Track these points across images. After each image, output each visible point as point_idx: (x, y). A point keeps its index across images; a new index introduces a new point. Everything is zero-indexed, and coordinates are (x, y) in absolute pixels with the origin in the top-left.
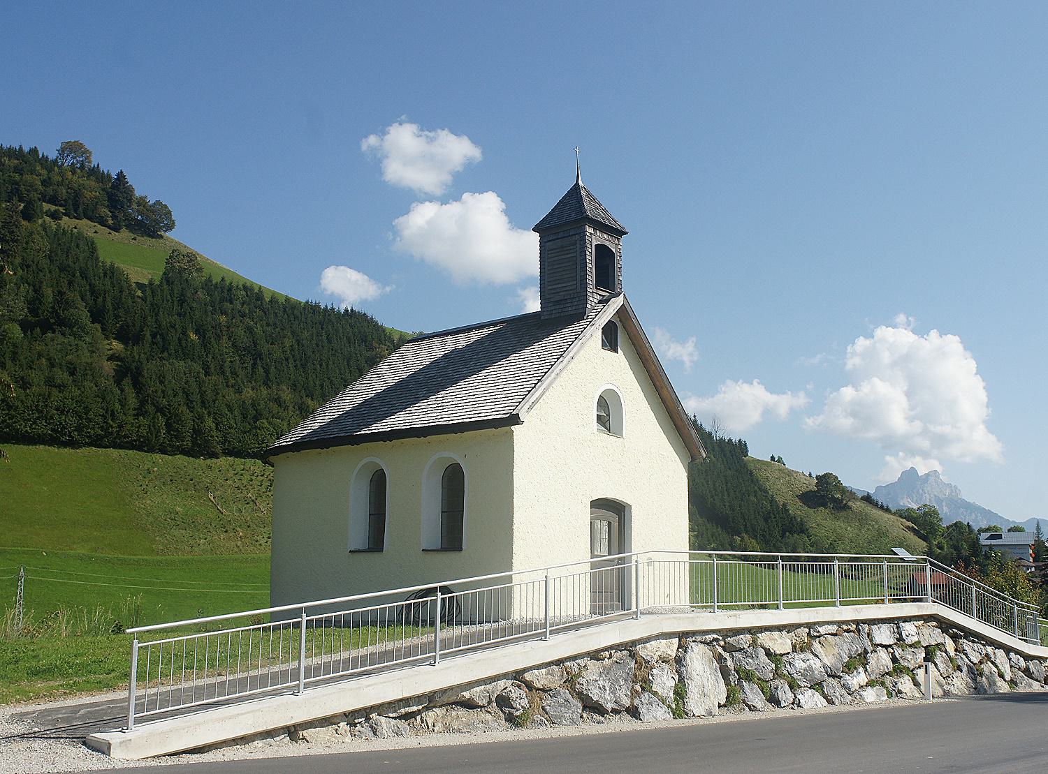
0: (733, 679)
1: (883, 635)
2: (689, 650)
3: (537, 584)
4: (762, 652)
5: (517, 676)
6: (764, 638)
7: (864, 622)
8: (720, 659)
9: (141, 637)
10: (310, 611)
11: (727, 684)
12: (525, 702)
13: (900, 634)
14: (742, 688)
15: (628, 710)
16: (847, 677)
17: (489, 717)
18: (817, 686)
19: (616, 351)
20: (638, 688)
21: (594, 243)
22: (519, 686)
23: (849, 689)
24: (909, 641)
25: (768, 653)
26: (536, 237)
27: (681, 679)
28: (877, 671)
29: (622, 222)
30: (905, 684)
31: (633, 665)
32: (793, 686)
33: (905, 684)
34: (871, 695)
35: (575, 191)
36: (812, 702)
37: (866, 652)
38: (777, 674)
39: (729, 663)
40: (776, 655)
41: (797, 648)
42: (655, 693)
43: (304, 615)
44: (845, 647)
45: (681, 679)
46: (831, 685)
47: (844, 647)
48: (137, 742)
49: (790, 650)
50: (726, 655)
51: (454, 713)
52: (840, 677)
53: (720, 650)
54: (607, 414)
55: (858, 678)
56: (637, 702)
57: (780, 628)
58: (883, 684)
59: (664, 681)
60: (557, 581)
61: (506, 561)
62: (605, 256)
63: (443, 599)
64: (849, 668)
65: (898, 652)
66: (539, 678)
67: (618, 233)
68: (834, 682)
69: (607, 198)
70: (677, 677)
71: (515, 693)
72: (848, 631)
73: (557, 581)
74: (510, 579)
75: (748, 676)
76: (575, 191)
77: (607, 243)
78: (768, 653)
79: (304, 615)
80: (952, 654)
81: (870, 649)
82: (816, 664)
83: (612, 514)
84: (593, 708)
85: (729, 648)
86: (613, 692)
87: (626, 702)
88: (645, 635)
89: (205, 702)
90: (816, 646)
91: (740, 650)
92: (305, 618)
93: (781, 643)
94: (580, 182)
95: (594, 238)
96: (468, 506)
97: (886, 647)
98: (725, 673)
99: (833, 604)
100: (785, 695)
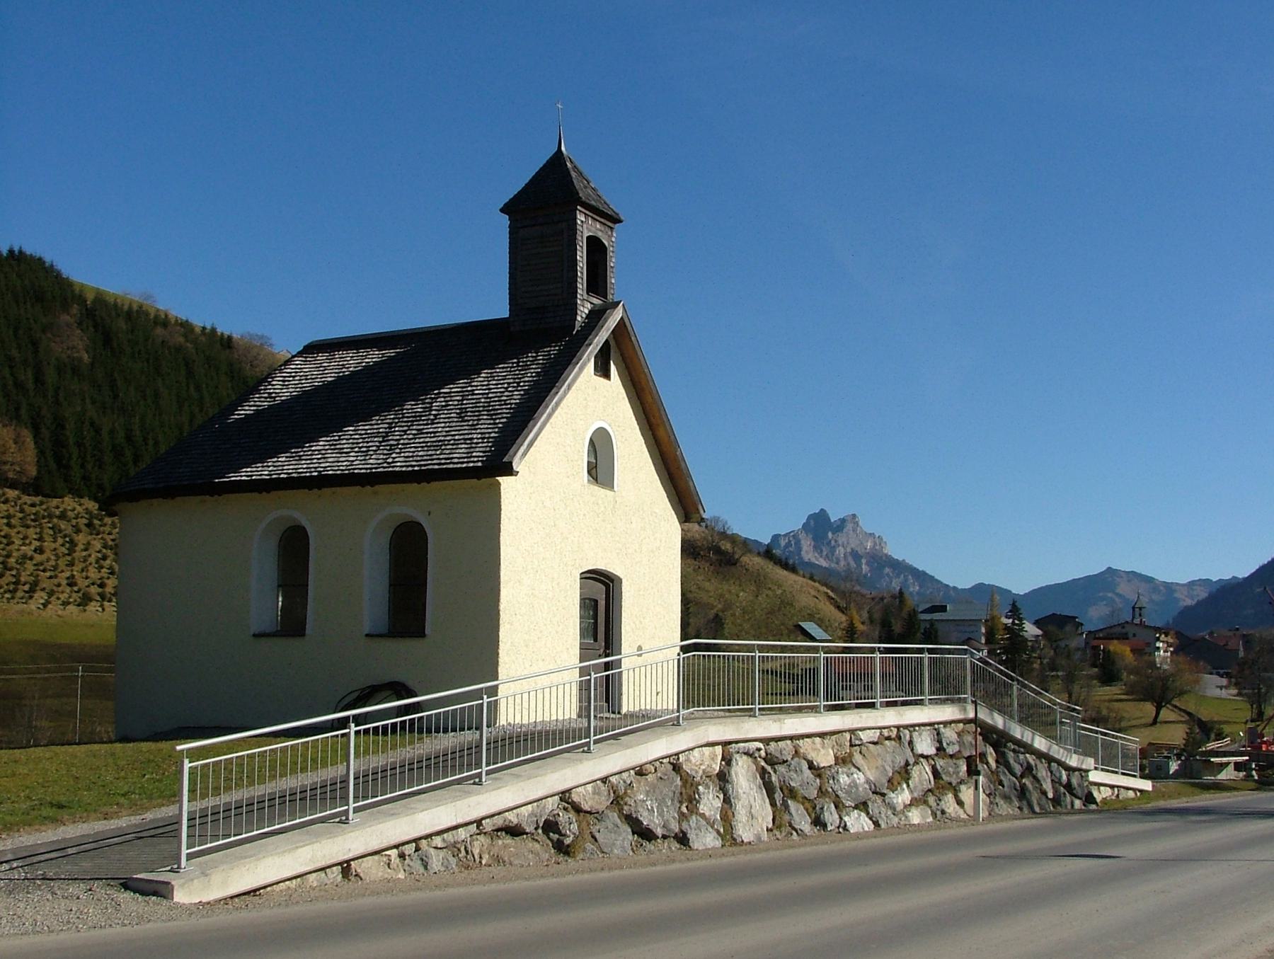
0: (778, 796)
1: (925, 745)
2: (734, 763)
3: (567, 686)
4: (805, 766)
5: (565, 796)
6: (805, 745)
7: (906, 727)
8: (763, 772)
9: (194, 754)
10: (358, 720)
11: (773, 804)
12: (574, 827)
13: (940, 742)
14: (787, 807)
15: (676, 837)
16: (892, 795)
17: (537, 846)
18: (863, 806)
19: (606, 374)
20: (684, 809)
21: (586, 234)
22: (565, 809)
23: (894, 809)
24: (950, 750)
25: (811, 766)
26: (505, 219)
27: (727, 800)
28: (920, 788)
29: (615, 204)
30: (949, 803)
31: (679, 782)
32: (838, 805)
33: (949, 803)
34: (915, 816)
35: (558, 158)
36: (858, 822)
37: (907, 764)
38: (822, 792)
39: (774, 778)
40: (819, 768)
41: (843, 761)
42: (703, 816)
43: (186, 761)
44: (889, 758)
45: (727, 800)
46: (876, 805)
47: (892, 757)
48: (208, 884)
49: (833, 762)
50: (769, 768)
51: (500, 842)
52: (883, 795)
53: (763, 763)
54: (600, 465)
55: (902, 797)
56: (685, 826)
57: (822, 735)
58: (926, 802)
59: (710, 803)
60: (511, 700)
61: (489, 667)
62: (597, 249)
63: (357, 733)
64: (892, 784)
65: (940, 763)
66: (585, 798)
67: (612, 219)
68: (878, 799)
69: (597, 174)
70: (721, 796)
71: (563, 818)
72: (888, 738)
73: (511, 700)
74: (493, 691)
75: (791, 793)
76: (558, 158)
77: (600, 234)
78: (811, 766)
79: (186, 761)
80: (993, 765)
81: (912, 761)
82: (859, 778)
83: (601, 602)
84: (644, 834)
85: (770, 760)
86: (661, 814)
87: (675, 827)
88: (454, 823)
89: (266, 830)
90: (857, 758)
91: (785, 762)
92: (353, 728)
93: (824, 756)
94: (563, 148)
95: (586, 226)
96: (428, 596)
97: (926, 757)
98: (769, 788)
99: (872, 706)
100: (831, 816)
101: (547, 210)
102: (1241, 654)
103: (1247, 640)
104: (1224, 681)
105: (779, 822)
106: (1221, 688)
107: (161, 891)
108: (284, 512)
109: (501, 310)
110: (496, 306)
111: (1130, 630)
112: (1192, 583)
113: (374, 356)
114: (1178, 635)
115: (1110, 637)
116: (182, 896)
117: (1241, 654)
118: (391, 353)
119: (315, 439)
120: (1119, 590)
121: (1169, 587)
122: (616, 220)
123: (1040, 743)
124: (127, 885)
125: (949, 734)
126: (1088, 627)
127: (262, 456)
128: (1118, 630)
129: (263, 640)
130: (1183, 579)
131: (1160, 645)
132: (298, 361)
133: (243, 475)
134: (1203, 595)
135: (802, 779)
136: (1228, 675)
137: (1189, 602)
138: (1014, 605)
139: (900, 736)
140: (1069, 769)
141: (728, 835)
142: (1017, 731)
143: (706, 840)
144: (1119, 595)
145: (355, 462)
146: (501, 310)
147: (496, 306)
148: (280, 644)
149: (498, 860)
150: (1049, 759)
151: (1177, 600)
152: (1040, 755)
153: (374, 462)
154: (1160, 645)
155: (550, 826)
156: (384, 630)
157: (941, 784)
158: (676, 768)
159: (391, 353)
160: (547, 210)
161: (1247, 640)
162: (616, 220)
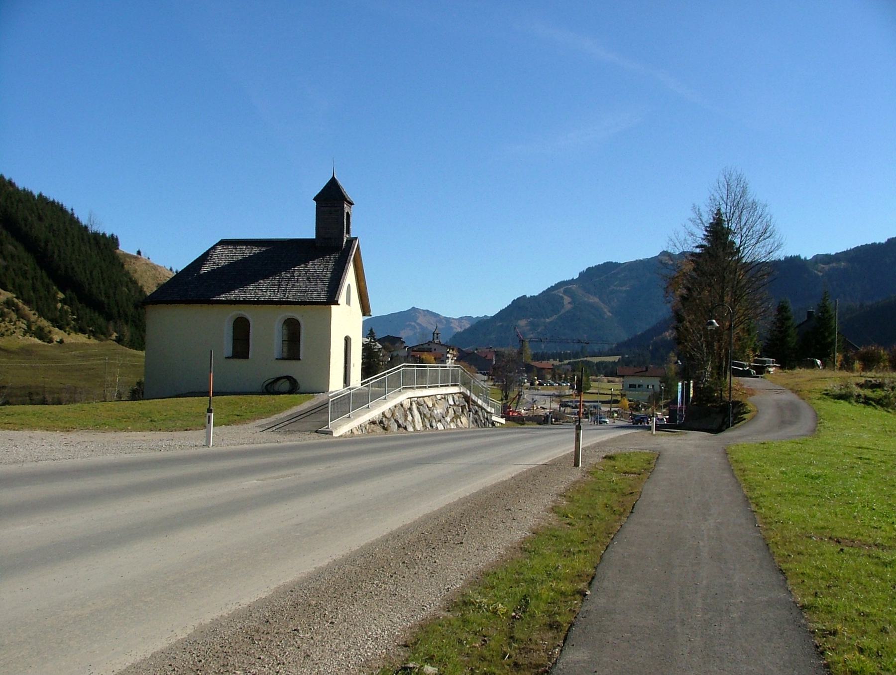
100: (434, 424)
101: (332, 201)
102: (494, 362)
103: (497, 354)
104: (486, 378)
105: (424, 426)
106: (485, 381)
107: (331, 433)
108: (239, 312)
109: (311, 234)
110: (310, 233)
111: (433, 346)
112: (462, 318)
113: (256, 250)
114: (459, 350)
115: (423, 351)
116: (335, 435)
117: (494, 362)
118: (264, 249)
119: (248, 284)
120: (418, 321)
121: (448, 320)
122: (352, 204)
123: (480, 402)
124: (316, 432)
125: (456, 397)
126: (409, 344)
127: (229, 290)
128: (426, 346)
129: (281, 361)
130: (457, 316)
131: (449, 355)
132: (220, 247)
133: (223, 297)
134: (468, 326)
135: (426, 411)
136: (488, 374)
137: (459, 330)
138: (371, 330)
139: (445, 397)
140: (488, 412)
141: (414, 427)
142: (474, 397)
143: (410, 429)
144: (418, 324)
145: (268, 295)
146: (311, 234)
147: (310, 233)
148: (287, 363)
149: (373, 431)
150: (482, 408)
151: (452, 328)
152: (479, 406)
153: (279, 296)
154: (449, 355)
155: (381, 422)
156: (285, 355)
157: (456, 417)
158: (402, 405)
159: (264, 249)
160: (332, 201)
161: (497, 354)
162: (352, 204)
